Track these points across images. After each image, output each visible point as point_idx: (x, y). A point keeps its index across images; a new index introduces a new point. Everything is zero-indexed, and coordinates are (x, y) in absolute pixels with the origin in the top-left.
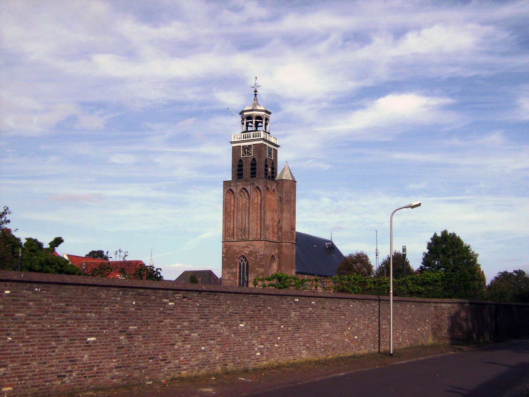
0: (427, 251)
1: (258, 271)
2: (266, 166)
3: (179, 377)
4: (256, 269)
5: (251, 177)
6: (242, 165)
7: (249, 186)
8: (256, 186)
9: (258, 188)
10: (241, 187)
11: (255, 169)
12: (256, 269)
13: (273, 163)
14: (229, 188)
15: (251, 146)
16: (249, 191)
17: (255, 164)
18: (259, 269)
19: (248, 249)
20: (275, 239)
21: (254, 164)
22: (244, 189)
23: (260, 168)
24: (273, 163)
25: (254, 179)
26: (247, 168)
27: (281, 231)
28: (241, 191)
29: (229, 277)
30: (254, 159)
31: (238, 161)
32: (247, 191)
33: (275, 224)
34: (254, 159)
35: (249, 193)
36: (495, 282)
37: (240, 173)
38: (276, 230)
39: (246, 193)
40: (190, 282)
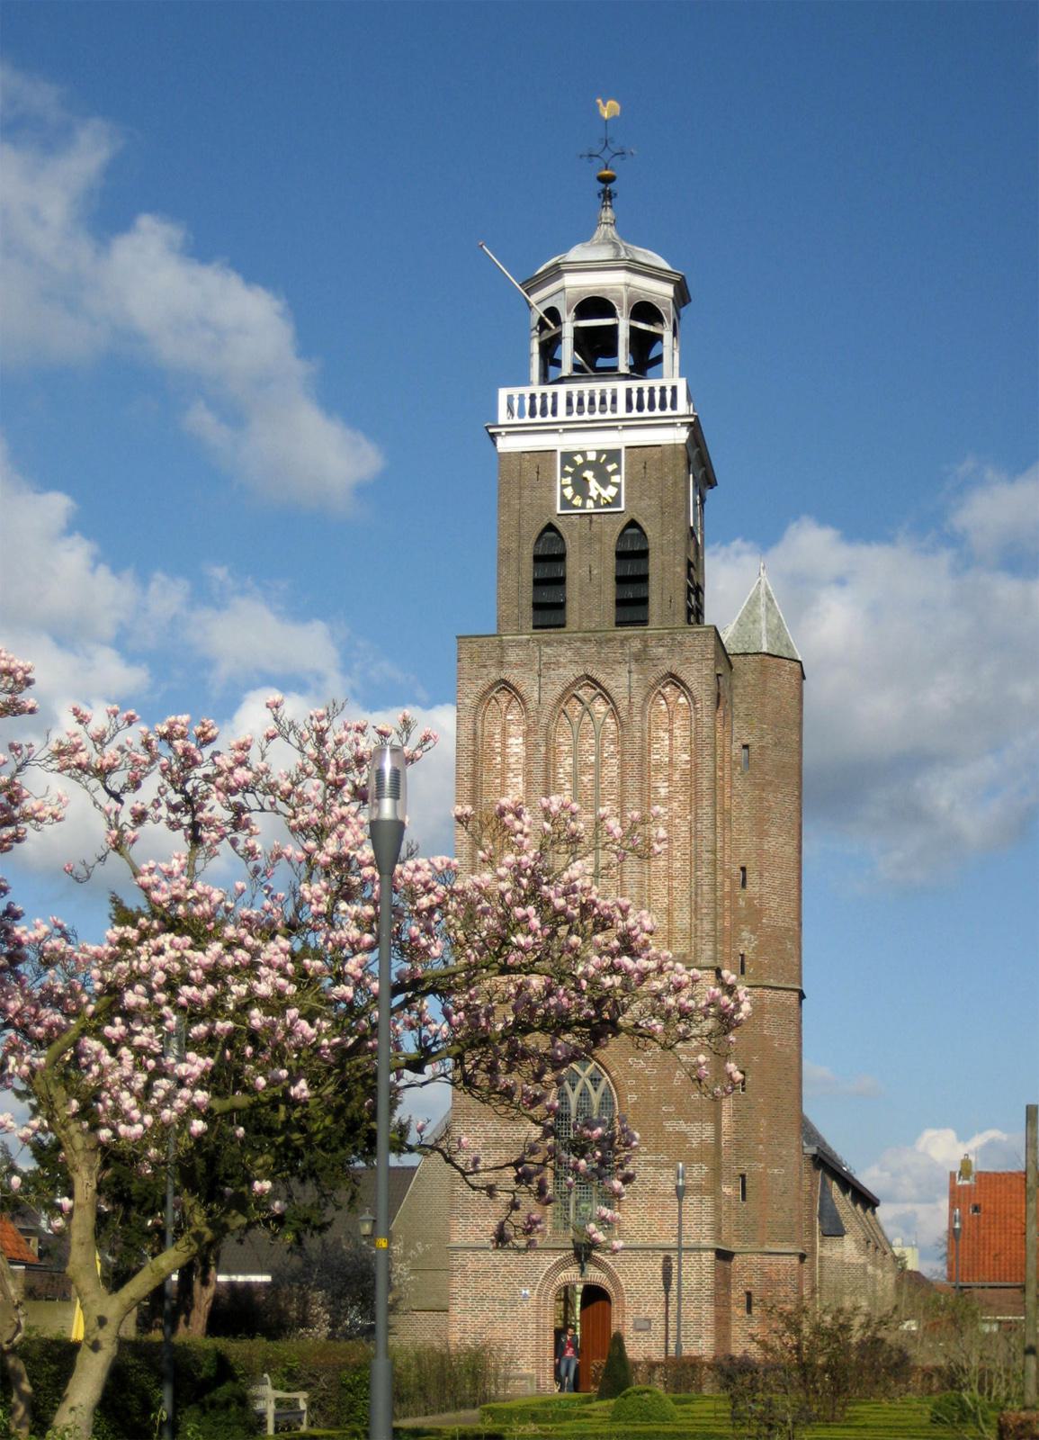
0: (58, 504)
1: (683, 1137)
3: (346, 670)
4: (670, 1126)
5: (619, 624)
7: (622, 670)
8: (664, 668)
9: (674, 679)
10: (571, 672)
12: (670, 1126)
14: (494, 674)
15: (613, 455)
16: (619, 693)
18: (683, 1126)
28: (568, 694)
32: (606, 695)
35: (623, 704)
37: (631, 569)
39: (600, 707)
40: (110, 1293)
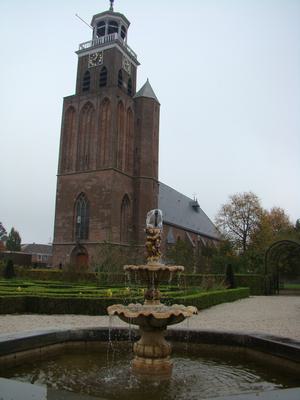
2: (120, 77)
4: (101, 211)
6: (89, 78)
10: (85, 101)
11: (105, 79)
13: (130, 80)
17: (105, 74)
18: (103, 211)
19: (90, 183)
20: (131, 174)
21: (104, 73)
22: (88, 103)
23: (113, 78)
24: (130, 80)
25: (104, 88)
26: (95, 79)
27: (139, 163)
29: (64, 224)
30: (104, 68)
31: (84, 72)
33: (132, 153)
34: (104, 68)
36: (95, 45)
38: (132, 161)
